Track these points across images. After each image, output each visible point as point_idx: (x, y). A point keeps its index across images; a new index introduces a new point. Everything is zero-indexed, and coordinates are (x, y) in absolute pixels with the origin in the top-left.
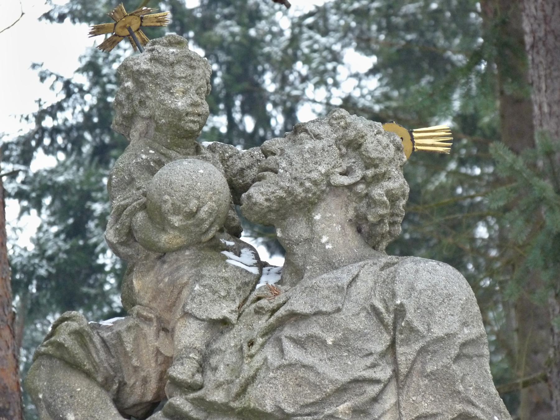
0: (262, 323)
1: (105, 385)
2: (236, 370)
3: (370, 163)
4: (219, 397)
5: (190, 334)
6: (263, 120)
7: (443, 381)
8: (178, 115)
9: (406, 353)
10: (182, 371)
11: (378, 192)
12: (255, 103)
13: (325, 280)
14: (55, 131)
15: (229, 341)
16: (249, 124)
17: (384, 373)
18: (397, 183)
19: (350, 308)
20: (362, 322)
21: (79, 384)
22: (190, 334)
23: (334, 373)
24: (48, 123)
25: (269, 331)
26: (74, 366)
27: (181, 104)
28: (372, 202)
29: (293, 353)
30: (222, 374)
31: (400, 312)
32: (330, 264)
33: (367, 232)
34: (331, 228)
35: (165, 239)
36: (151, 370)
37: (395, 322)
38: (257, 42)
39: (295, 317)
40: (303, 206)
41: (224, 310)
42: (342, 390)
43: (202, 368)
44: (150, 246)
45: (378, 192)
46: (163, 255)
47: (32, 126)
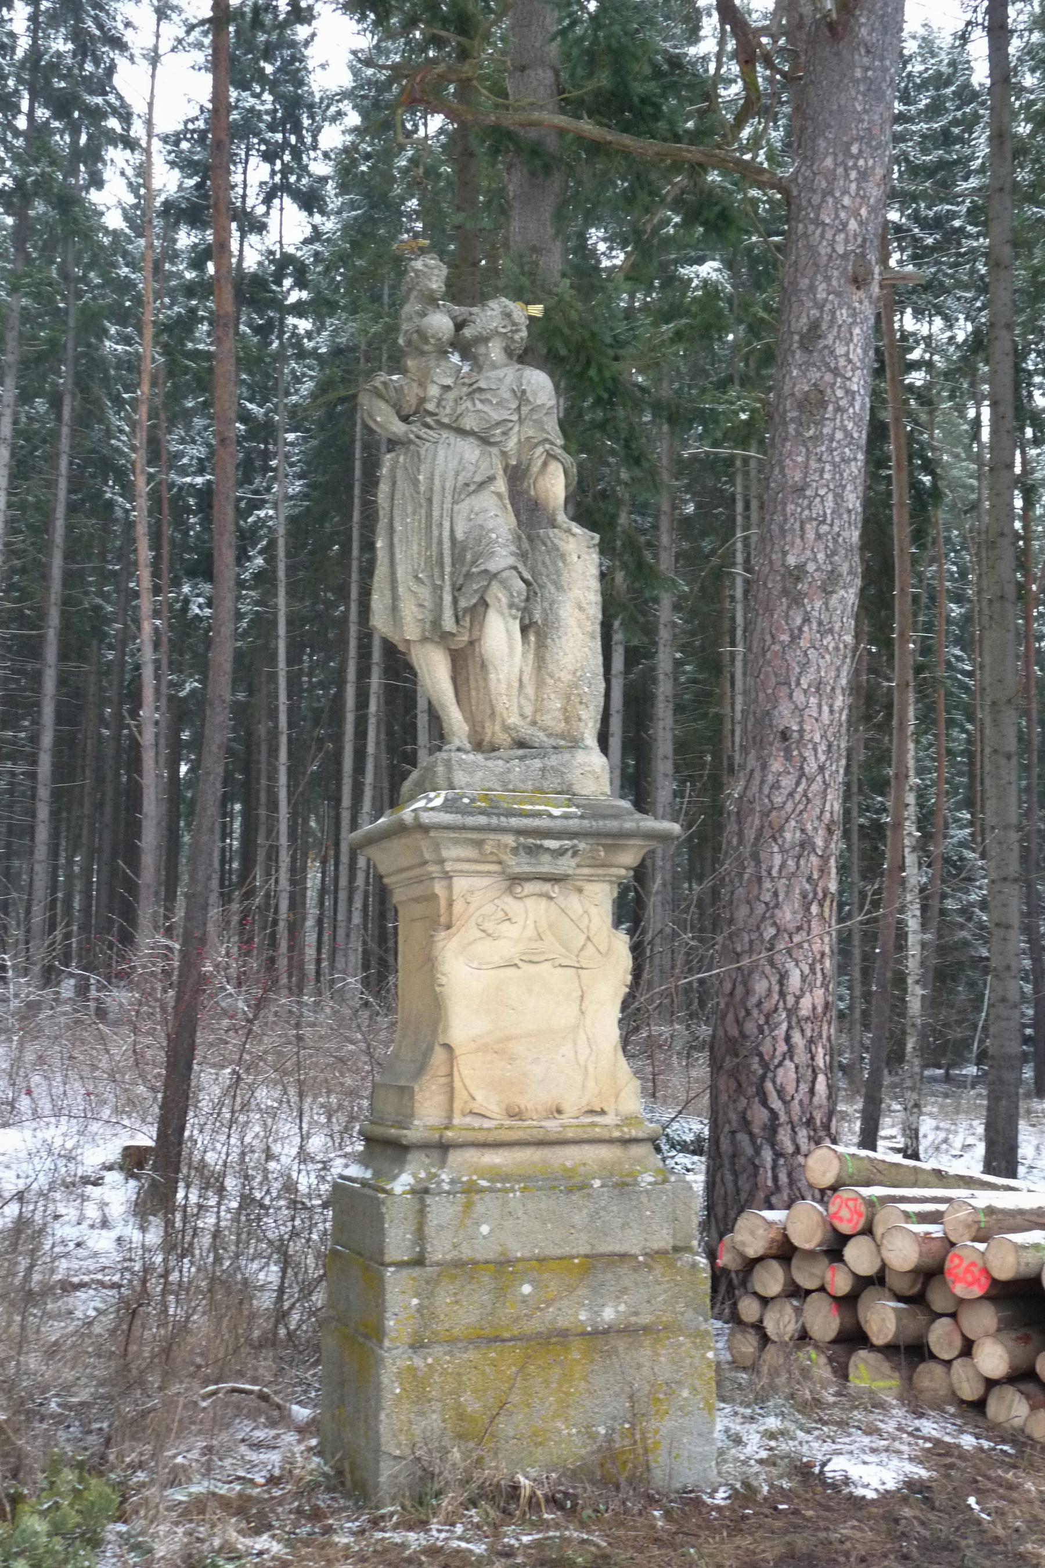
0: (465, 390)
1: (394, 406)
2: (454, 410)
3: (514, 324)
4: (446, 420)
5: (434, 391)
6: (301, 138)
7: (539, 424)
8: (433, 291)
9: (525, 410)
10: (430, 406)
11: (517, 337)
12: (297, 129)
13: (493, 374)
14: (193, 131)
15: (451, 396)
16: (293, 139)
17: (515, 418)
18: (524, 334)
19: (504, 388)
20: (507, 395)
21: (383, 405)
22: (434, 391)
23: (496, 416)
24: (190, 126)
25: (469, 394)
26: (381, 396)
27: (434, 286)
28: (514, 341)
29: (479, 406)
30: (448, 411)
31: (524, 392)
32: (494, 366)
33: (509, 352)
34: (495, 351)
35: (426, 348)
36: (414, 402)
37: (521, 396)
38: (301, 97)
39: (480, 390)
40: (483, 339)
41: (449, 382)
42: (498, 424)
43: (438, 405)
44: (417, 349)
45: (517, 337)
46: (423, 353)
47: (181, 127)
